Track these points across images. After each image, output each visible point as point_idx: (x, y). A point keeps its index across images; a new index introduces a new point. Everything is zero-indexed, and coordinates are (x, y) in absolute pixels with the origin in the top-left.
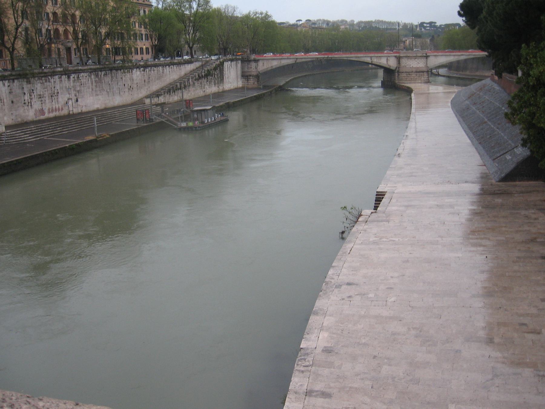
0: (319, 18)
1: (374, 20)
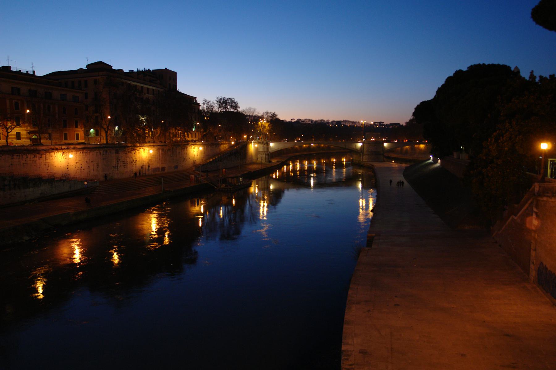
0: (306, 118)
1: (342, 120)
